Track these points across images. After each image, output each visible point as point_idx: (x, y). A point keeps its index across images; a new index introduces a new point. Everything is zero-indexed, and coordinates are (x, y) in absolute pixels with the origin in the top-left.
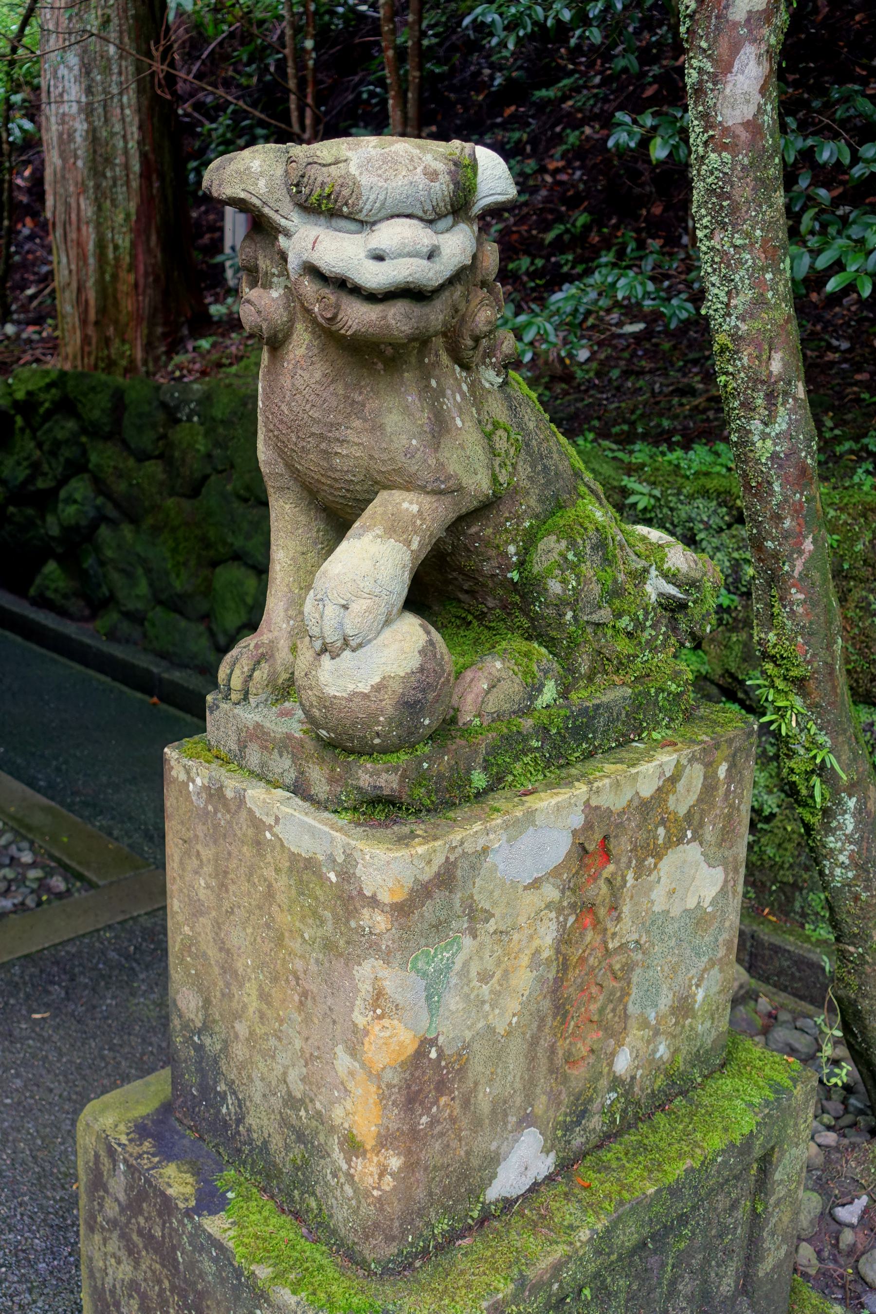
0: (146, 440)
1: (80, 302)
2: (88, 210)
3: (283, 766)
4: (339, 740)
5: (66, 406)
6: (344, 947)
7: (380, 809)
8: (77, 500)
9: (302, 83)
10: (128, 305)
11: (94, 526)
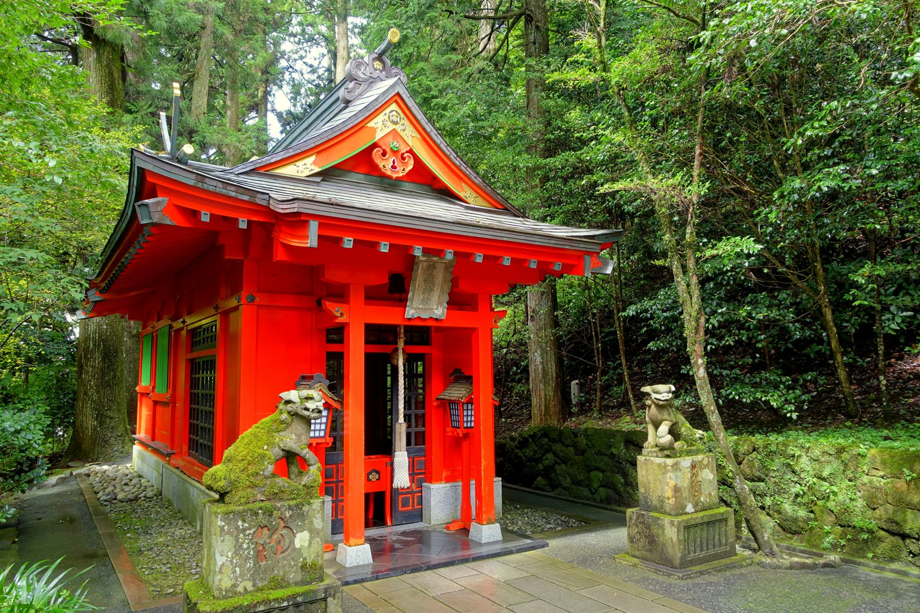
0: (569, 442)
2: (542, 387)
3: (655, 454)
4: (662, 449)
6: (664, 473)
7: (668, 456)
10: (552, 410)
11: (554, 465)
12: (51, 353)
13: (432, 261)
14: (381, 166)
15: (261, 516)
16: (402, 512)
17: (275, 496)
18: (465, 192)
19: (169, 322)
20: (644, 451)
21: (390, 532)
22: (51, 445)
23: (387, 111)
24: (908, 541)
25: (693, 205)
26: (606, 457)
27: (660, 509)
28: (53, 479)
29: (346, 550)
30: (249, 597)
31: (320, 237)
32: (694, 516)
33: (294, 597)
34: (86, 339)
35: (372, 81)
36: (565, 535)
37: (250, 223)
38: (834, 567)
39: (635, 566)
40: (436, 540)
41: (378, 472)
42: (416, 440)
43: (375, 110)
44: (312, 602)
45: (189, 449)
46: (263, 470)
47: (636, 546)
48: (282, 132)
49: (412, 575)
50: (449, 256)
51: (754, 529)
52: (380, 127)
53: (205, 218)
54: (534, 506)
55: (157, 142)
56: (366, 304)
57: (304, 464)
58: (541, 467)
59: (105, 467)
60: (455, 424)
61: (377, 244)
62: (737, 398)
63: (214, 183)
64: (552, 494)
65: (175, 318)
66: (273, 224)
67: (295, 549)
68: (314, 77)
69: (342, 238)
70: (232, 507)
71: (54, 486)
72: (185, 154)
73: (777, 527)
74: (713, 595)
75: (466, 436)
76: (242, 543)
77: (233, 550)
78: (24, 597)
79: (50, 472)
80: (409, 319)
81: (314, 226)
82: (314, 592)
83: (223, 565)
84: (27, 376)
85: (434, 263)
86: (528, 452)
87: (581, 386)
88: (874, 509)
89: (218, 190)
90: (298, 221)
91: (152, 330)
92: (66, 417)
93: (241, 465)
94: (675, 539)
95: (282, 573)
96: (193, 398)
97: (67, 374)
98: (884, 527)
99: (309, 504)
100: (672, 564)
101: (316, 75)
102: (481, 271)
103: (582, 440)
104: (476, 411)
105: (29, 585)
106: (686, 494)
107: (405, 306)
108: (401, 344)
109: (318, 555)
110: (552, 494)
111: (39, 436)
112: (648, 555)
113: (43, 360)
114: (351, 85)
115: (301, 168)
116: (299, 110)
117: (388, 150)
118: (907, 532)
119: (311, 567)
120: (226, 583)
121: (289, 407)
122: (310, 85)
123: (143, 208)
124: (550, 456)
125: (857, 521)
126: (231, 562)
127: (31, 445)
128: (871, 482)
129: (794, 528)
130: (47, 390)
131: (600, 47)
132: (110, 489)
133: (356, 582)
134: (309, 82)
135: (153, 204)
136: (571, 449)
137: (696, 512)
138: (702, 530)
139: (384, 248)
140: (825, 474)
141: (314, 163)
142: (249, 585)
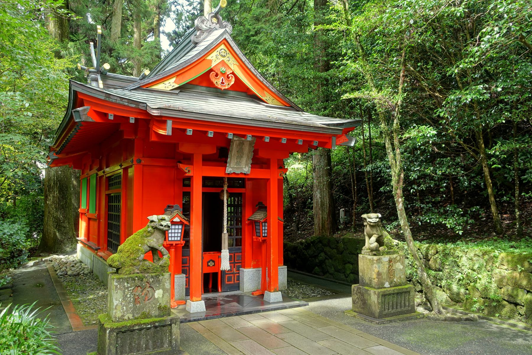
1: (319, 226)
2: (320, 212)
4: (372, 250)
5: (320, 242)
6: (372, 265)
7: (375, 255)
8: (322, 256)
9: (355, 193)
10: (326, 226)
12: (28, 188)
13: (242, 140)
14: (215, 83)
15: (137, 281)
16: (227, 285)
17: (145, 271)
18: (266, 97)
19: (96, 172)
20: (363, 252)
21: (220, 295)
22: (30, 243)
23: (219, 49)
24: (518, 307)
25: (398, 106)
26: (354, 255)
27: (369, 285)
28: (31, 263)
29: (190, 303)
30: (130, 322)
31: (173, 129)
32: (388, 289)
33: (154, 323)
34: (49, 180)
35: (210, 31)
36: (321, 300)
37: (136, 119)
38: (472, 320)
39: (354, 316)
40: (246, 300)
41: (213, 261)
42: (237, 244)
43: (210, 50)
44: (164, 326)
45: (108, 246)
46: (138, 257)
47: (356, 305)
48: (170, 45)
49: (227, 318)
50: (249, 138)
51: (429, 298)
52: (214, 59)
53: (111, 118)
54: (308, 283)
55: (89, 61)
56: (203, 165)
57: (162, 255)
58: (317, 261)
59: (61, 256)
60: (258, 234)
61: (206, 132)
62: (428, 221)
63: (116, 98)
64: (323, 277)
65: (100, 169)
66: (150, 120)
67: (155, 298)
68: (190, 8)
69: (186, 130)
70: (122, 276)
71: (32, 266)
72: (105, 69)
73: (448, 298)
74: (392, 332)
75: (264, 241)
76: (127, 294)
77: (122, 298)
78: (17, 320)
79: (29, 259)
80: (228, 174)
81: (170, 123)
82: (165, 321)
83: (117, 305)
84: (15, 201)
85: (243, 141)
86: (310, 252)
87: (346, 212)
88: (501, 288)
89: (118, 102)
90: (161, 121)
91: (87, 176)
92: (39, 226)
93: (127, 254)
94: (376, 302)
95: (148, 311)
96: (109, 217)
97: (39, 200)
98: (506, 299)
99: (163, 275)
100: (374, 315)
101: (192, 7)
102: (272, 145)
103: (341, 245)
104: (271, 226)
105: (20, 316)
106: (385, 276)
107: (226, 167)
108: (225, 188)
109: (167, 302)
110: (323, 277)
111: (23, 237)
112: (362, 311)
113: (25, 193)
114: (198, 33)
115: (167, 85)
116: (181, 30)
117: (219, 73)
118: (518, 302)
119: (164, 308)
120: (119, 314)
121: (152, 224)
122: (188, 14)
123: (76, 113)
124: (323, 254)
125: (492, 295)
126: (121, 304)
127: (19, 242)
128: (500, 273)
129: (457, 299)
130: (26, 209)
131: (345, 10)
132: (64, 268)
133: (195, 320)
134: (187, 12)
135: (82, 110)
136: (335, 250)
137: (391, 287)
138: (394, 297)
139: (211, 135)
140: (475, 267)
141: (175, 82)
142: (131, 316)
